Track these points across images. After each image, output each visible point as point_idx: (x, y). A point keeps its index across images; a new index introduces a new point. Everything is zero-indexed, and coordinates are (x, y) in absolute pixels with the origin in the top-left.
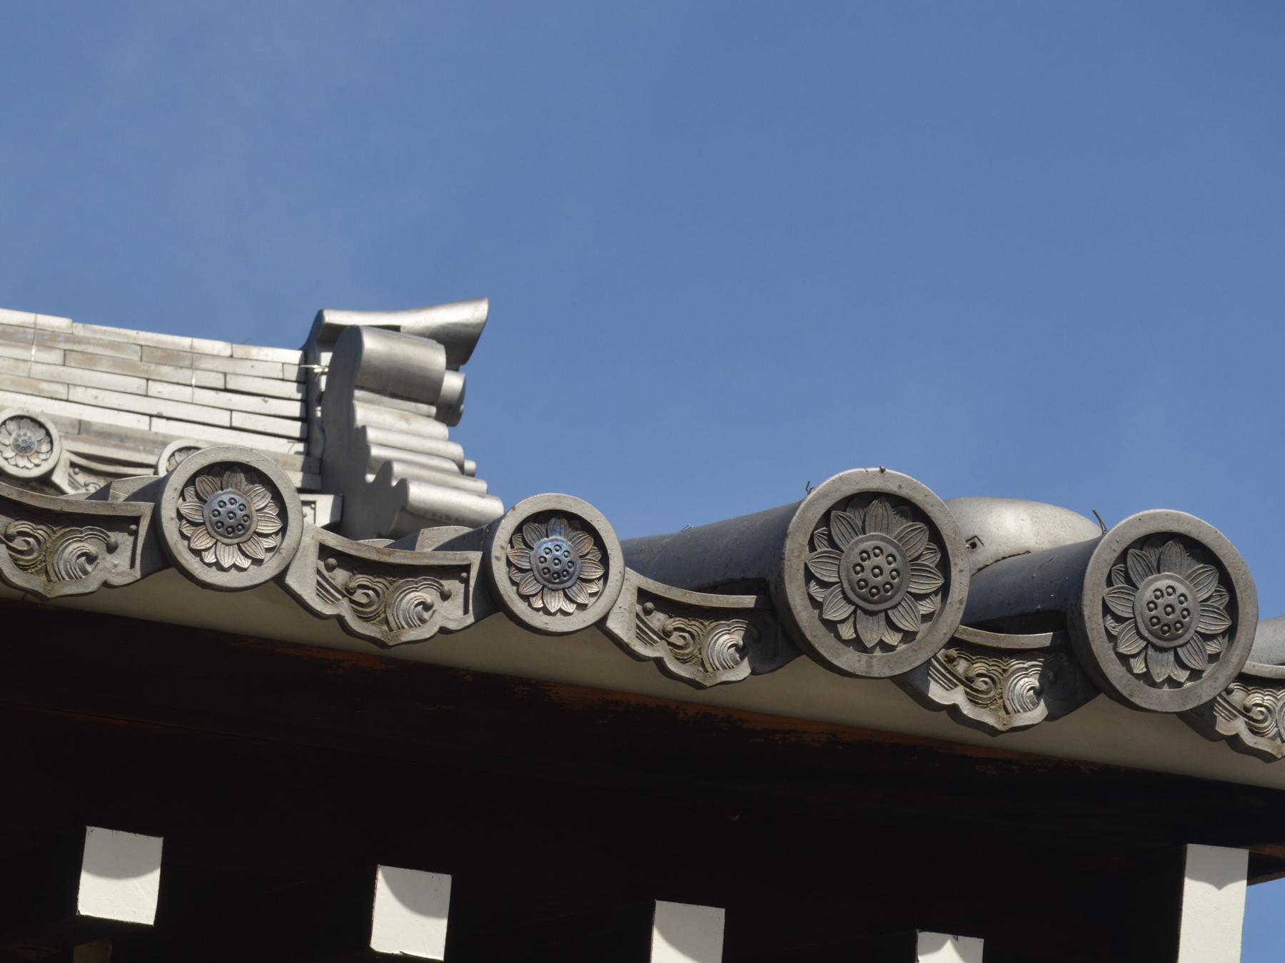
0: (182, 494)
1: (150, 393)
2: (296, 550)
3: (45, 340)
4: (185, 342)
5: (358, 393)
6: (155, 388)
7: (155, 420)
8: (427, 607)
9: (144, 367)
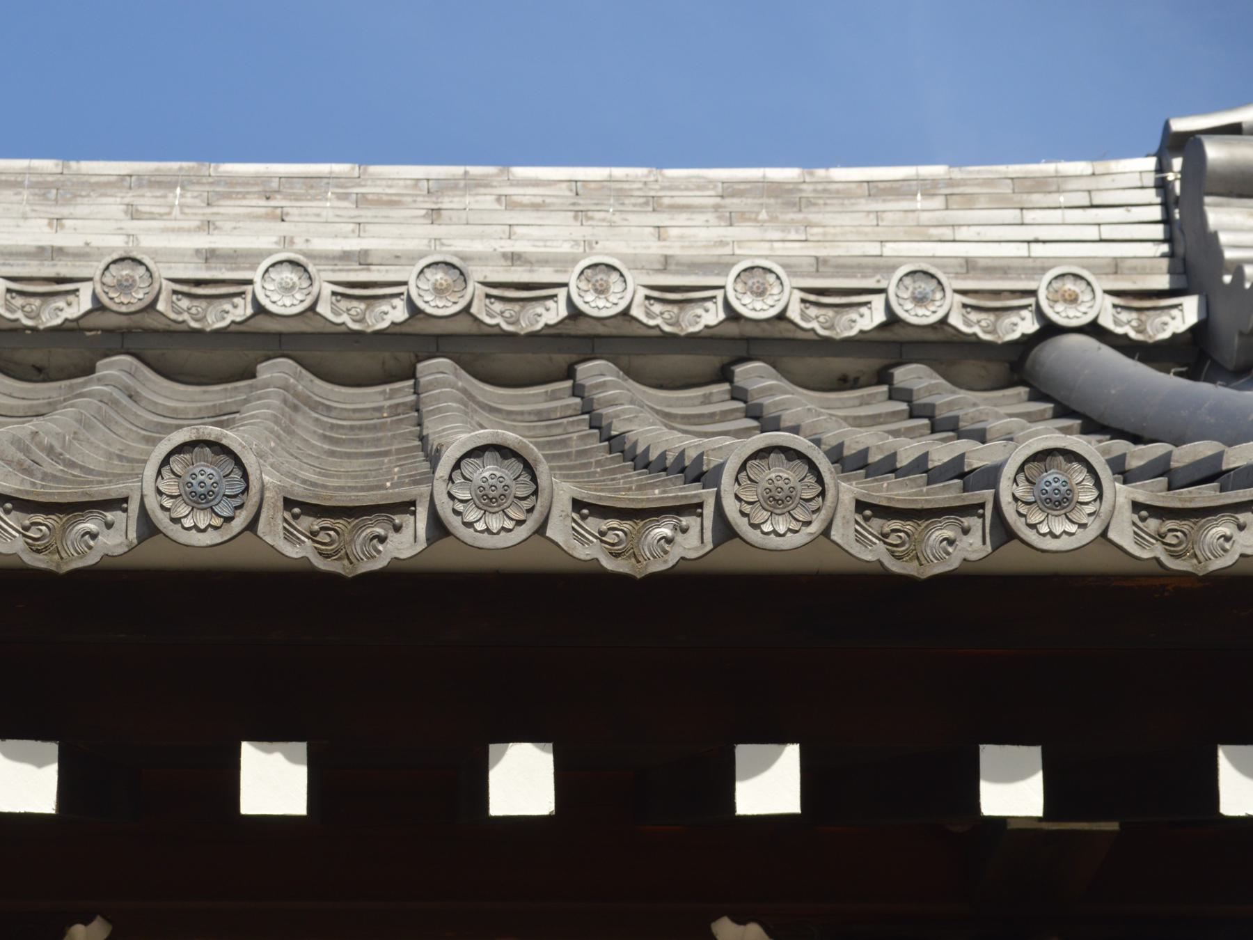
0: (1015, 480)
1: (1026, 221)
2: (1114, 507)
3: (929, 188)
4: (1048, 168)
5: (1208, 200)
6: (1030, 216)
7: (1033, 246)
8: (1227, 539)
9: (1017, 198)
